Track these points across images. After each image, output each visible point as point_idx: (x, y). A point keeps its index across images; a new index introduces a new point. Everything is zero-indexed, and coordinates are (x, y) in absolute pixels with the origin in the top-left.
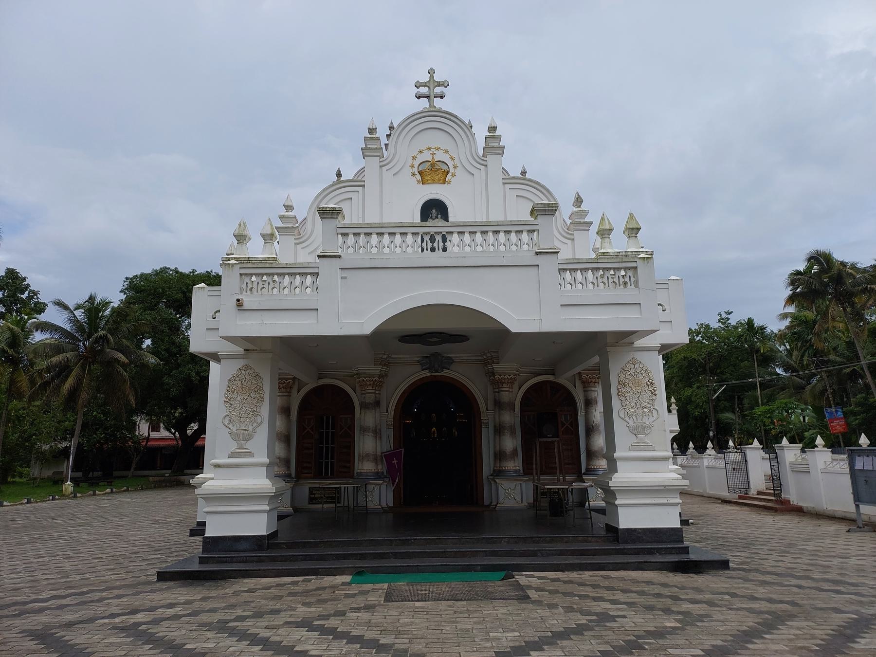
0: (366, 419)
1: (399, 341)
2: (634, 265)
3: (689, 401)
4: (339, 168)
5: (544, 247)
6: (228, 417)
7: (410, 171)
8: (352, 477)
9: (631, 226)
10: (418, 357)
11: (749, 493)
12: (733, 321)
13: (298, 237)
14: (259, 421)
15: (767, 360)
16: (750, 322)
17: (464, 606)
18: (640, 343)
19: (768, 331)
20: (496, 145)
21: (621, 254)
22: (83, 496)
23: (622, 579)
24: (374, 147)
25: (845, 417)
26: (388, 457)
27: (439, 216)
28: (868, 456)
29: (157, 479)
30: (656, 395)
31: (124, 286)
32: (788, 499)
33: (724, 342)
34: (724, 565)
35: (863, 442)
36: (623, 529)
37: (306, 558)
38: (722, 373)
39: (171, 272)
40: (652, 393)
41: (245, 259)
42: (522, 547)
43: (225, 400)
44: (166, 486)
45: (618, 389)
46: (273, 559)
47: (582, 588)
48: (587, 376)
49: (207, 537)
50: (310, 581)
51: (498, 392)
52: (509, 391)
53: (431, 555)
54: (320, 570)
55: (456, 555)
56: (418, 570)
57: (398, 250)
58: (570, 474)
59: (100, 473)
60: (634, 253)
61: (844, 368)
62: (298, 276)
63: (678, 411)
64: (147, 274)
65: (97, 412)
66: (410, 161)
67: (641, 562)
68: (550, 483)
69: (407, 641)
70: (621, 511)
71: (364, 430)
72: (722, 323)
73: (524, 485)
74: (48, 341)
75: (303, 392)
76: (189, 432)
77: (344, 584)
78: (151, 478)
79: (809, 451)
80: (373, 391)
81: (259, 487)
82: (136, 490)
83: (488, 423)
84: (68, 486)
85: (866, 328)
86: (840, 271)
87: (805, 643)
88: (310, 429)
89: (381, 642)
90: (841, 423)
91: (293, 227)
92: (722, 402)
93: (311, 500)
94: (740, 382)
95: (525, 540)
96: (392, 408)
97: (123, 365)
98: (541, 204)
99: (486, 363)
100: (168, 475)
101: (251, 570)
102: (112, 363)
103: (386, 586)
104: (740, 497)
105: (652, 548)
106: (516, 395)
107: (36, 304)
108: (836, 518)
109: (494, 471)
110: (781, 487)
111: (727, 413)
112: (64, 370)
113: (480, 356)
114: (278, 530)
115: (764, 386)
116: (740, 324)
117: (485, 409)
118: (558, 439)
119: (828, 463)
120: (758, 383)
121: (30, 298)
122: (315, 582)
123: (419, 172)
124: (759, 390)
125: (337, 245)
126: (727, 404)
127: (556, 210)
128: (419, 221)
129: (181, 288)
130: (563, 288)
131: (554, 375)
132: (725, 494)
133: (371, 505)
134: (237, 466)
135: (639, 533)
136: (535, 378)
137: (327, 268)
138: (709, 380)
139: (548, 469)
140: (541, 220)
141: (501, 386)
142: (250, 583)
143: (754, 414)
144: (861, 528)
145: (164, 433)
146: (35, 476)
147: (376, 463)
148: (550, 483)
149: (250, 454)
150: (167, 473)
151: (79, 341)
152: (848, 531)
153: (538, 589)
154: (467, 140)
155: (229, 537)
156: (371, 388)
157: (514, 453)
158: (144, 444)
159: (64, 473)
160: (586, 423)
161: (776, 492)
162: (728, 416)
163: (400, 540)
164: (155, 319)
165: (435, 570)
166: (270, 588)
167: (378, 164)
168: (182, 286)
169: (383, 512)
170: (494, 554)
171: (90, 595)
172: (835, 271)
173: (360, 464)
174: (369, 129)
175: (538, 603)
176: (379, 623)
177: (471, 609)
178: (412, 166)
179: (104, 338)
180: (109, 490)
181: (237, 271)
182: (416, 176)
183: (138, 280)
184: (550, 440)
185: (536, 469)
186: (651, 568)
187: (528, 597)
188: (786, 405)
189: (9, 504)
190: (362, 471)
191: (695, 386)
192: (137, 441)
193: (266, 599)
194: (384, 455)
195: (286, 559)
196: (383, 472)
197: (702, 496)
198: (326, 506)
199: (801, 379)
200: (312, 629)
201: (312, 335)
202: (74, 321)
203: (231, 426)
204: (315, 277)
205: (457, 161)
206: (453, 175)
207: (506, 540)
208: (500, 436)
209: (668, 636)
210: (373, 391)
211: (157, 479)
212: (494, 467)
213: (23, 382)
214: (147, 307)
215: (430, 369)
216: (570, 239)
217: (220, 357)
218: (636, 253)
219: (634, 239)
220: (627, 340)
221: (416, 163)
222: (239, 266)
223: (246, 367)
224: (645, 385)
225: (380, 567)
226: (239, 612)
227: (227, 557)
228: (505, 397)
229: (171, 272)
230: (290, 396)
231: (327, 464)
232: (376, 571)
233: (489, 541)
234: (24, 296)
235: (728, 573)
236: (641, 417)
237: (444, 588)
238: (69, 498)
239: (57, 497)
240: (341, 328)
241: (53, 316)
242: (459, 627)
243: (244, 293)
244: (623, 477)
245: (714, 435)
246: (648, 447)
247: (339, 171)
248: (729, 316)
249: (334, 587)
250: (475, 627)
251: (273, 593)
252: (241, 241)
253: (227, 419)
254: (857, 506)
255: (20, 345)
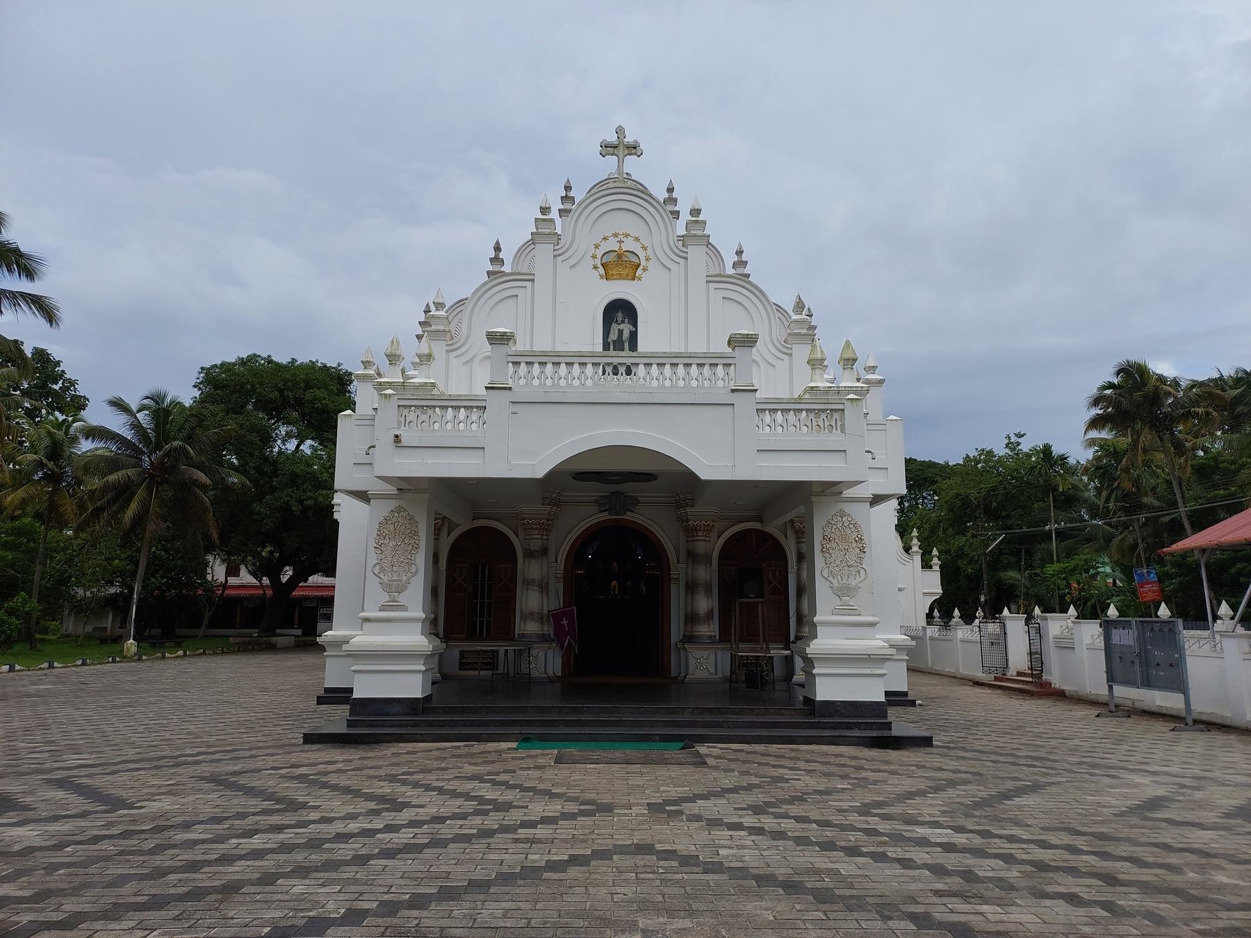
0: (531, 570)
1: (573, 478)
2: (841, 407)
3: (961, 554)
4: (498, 240)
5: (741, 383)
6: (378, 565)
7: (592, 262)
8: (513, 639)
9: (846, 356)
10: (595, 496)
11: (1007, 674)
12: (1025, 447)
13: (451, 342)
14: (414, 571)
15: (1069, 501)
16: (1047, 450)
17: (637, 768)
18: (849, 493)
19: (1072, 461)
20: (699, 233)
21: (832, 389)
22: (149, 659)
23: (813, 752)
24: (547, 231)
25: (1160, 581)
26: (556, 617)
27: (626, 320)
28: (1124, 629)
29: (239, 640)
30: (864, 552)
31: (198, 378)
32: (1049, 681)
33: (1011, 476)
34: (926, 742)
35: (1162, 613)
36: (820, 701)
37: (466, 724)
38: (1009, 516)
39: (263, 362)
40: (860, 550)
41: (400, 384)
42: (708, 718)
43: (375, 545)
44: (253, 650)
45: (822, 545)
46: (430, 724)
47: (764, 758)
48: (801, 524)
49: (354, 699)
50: (473, 746)
51: (693, 541)
52: (706, 541)
53: (604, 724)
54: (483, 736)
55: (632, 724)
56: (591, 738)
57: (576, 382)
58: (776, 642)
59: (159, 630)
60: (847, 389)
61: (1163, 515)
62: (462, 410)
63: (941, 567)
64: (229, 364)
65: (157, 548)
66: (592, 251)
67: (836, 736)
68: (746, 651)
69: (580, 791)
70: (818, 680)
71: (528, 583)
72: (1010, 448)
73: (719, 653)
74: (100, 452)
75: (456, 533)
76: (284, 579)
77: (509, 749)
78: (231, 638)
79: (1084, 623)
80: (539, 537)
81: (414, 644)
82: (215, 654)
83: (679, 578)
84: (131, 645)
85: (1189, 465)
86: (1156, 388)
87: (962, 800)
88: (463, 580)
89: (553, 791)
90: (1154, 588)
91: (444, 331)
92: (1005, 556)
93: (462, 666)
94: (1033, 529)
95: (710, 710)
96: (562, 556)
97: (204, 487)
98: (740, 334)
99: (678, 505)
100: (256, 635)
101: (407, 734)
102: (188, 486)
103: (555, 751)
104: (996, 679)
105: (850, 723)
106: (714, 546)
107: (74, 397)
108: (1099, 703)
109: (684, 636)
110: (1042, 667)
111: (1011, 572)
112: (123, 493)
113: (672, 497)
114: (431, 695)
115: (1061, 535)
116: (1034, 451)
117: (675, 559)
118: (762, 600)
119: (1095, 637)
120: (1054, 532)
121: (65, 389)
122: (477, 747)
123: (602, 265)
124: (1054, 542)
125: (507, 375)
126: (1012, 559)
127: (756, 341)
128: (602, 350)
129: (277, 384)
130: (761, 431)
131: (761, 521)
132: (979, 675)
133: (534, 673)
134: (389, 620)
135: (839, 706)
136: (736, 526)
137: (497, 402)
138: (983, 527)
139: (750, 636)
140: (739, 352)
141: (695, 534)
142: (410, 746)
143: (1046, 574)
144: (1112, 712)
145: (246, 577)
146: (69, 632)
147: (542, 623)
148: (746, 651)
149: (402, 608)
150: (255, 633)
151: (144, 453)
152: (1098, 716)
153: (716, 757)
154: (663, 228)
155: (379, 698)
156: (537, 532)
157: (710, 615)
158: (220, 592)
159: (109, 629)
160: (797, 582)
161: (1034, 672)
162: (1012, 575)
163: (570, 707)
164: (241, 426)
165: (611, 739)
166: (431, 751)
167: (552, 253)
168: (278, 382)
169: (549, 682)
170: (676, 724)
171: (238, 752)
172: (1150, 388)
173: (523, 624)
174: (541, 208)
175: (716, 768)
176: (550, 779)
177: (645, 770)
178: (594, 257)
179: (181, 451)
180: (180, 653)
181: (395, 402)
182: (599, 269)
183: (217, 371)
184: (752, 600)
185: (735, 636)
186: (846, 743)
187: (706, 763)
188: (1086, 563)
189: (60, 665)
190: (525, 632)
191: (969, 534)
192: (210, 588)
193: (430, 759)
194: (552, 615)
195: (443, 724)
196: (550, 635)
197: (954, 677)
198: (482, 673)
199: (1113, 528)
200: (482, 781)
201: (478, 476)
202: (136, 426)
203: (381, 575)
204: (482, 411)
205: (650, 252)
206: (645, 269)
207: (690, 710)
208: (692, 594)
209: (834, 794)
210: (539, 537)
211: (239, 640)
212: (685, 631)
213: (68, 506)
214: (231, 409)
215: (610, 511)
216: (787, 354)
217: (370, 496)
218: (850, 389)
219: (849, 370)
220: (834, 489)
221: (599, 253)
222: (397, 397)
223: (399, 510)
224: (853, 541)
225: (550, 734)
226: (405, 769)
227: (378, 720)
228: (701, 547)
229: (263, 362)
230: (438, 539)
231: (482, 622)
232: (544, 738)
233: (673, 711)
234: (56, 387)
235: (930, 750)
236: (847, 576)
237: (618, 754)
238: (134, 661)
239: (118, 659)
240: (510, 470)
241: (98, 414)
242: (630, 783)
243: (403, 427)
244: (824, 642)
245: (986, 600)
246: (853, 611)
247: (498, 243)
248: (1020, 440)
249: (500, 752)
250: (647, 782)
251: (434, 755)
252: (394, 362)
253: (378, 567)
254: (1111, 687)
255: (62, 456)
